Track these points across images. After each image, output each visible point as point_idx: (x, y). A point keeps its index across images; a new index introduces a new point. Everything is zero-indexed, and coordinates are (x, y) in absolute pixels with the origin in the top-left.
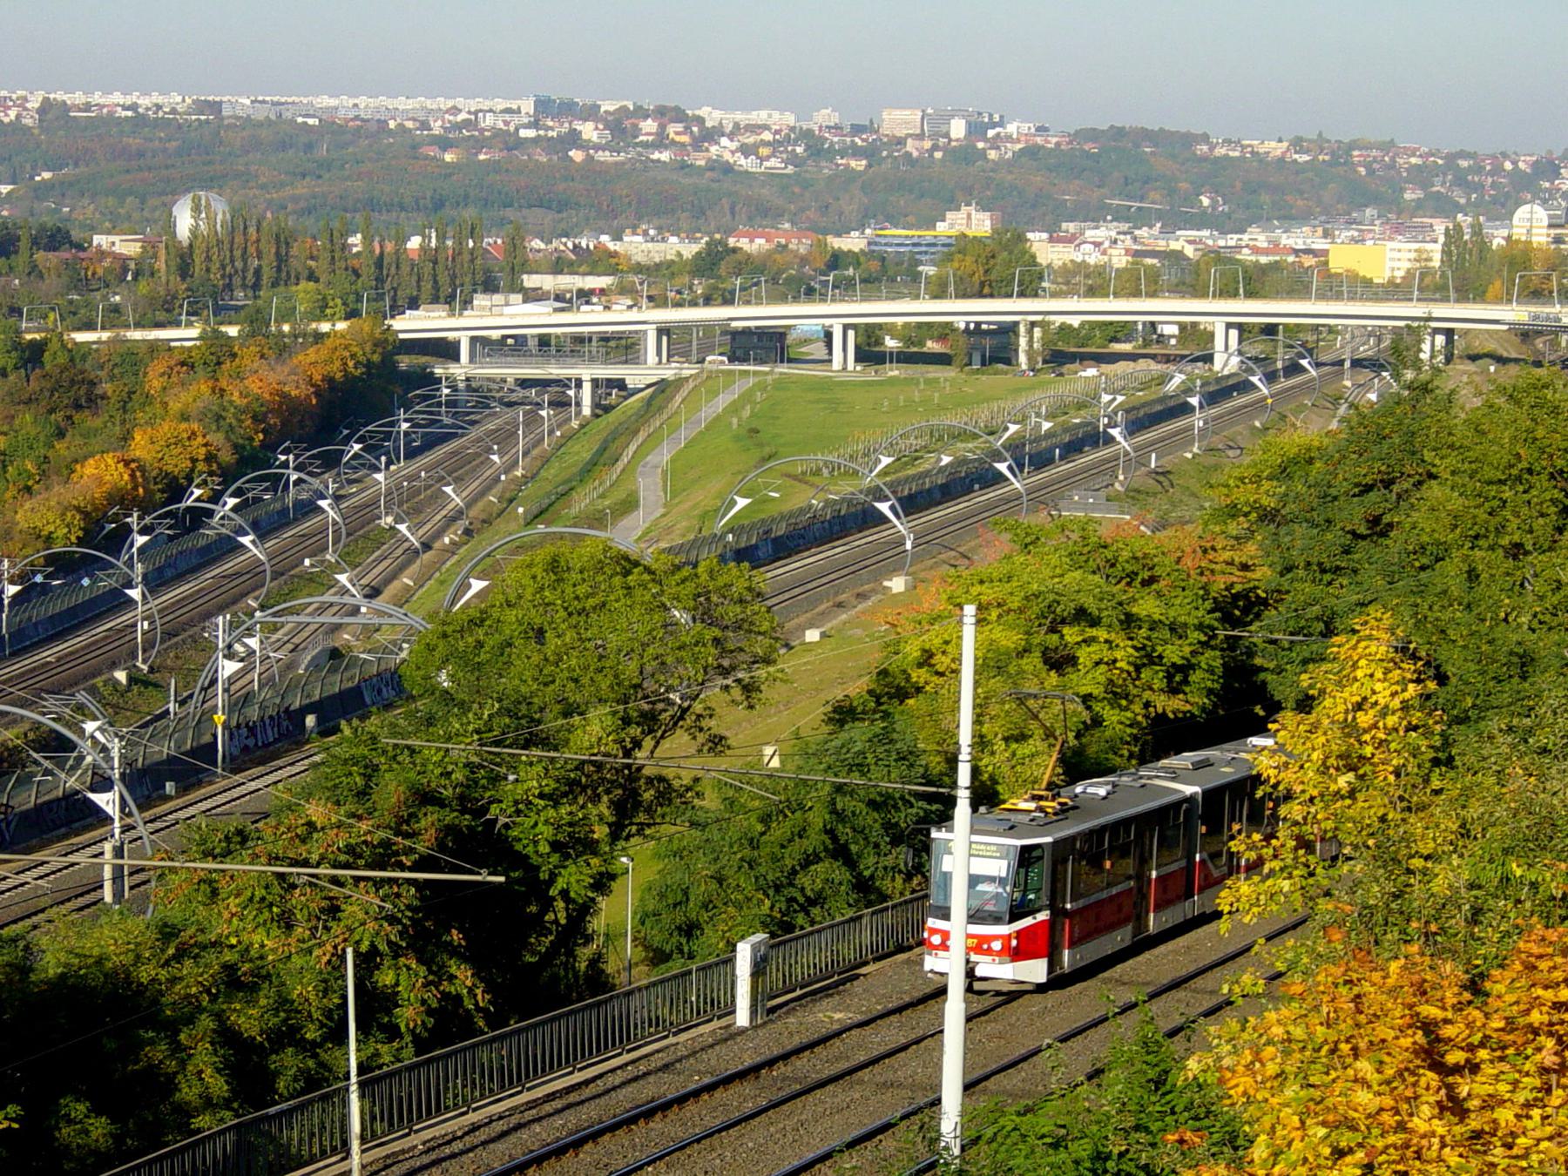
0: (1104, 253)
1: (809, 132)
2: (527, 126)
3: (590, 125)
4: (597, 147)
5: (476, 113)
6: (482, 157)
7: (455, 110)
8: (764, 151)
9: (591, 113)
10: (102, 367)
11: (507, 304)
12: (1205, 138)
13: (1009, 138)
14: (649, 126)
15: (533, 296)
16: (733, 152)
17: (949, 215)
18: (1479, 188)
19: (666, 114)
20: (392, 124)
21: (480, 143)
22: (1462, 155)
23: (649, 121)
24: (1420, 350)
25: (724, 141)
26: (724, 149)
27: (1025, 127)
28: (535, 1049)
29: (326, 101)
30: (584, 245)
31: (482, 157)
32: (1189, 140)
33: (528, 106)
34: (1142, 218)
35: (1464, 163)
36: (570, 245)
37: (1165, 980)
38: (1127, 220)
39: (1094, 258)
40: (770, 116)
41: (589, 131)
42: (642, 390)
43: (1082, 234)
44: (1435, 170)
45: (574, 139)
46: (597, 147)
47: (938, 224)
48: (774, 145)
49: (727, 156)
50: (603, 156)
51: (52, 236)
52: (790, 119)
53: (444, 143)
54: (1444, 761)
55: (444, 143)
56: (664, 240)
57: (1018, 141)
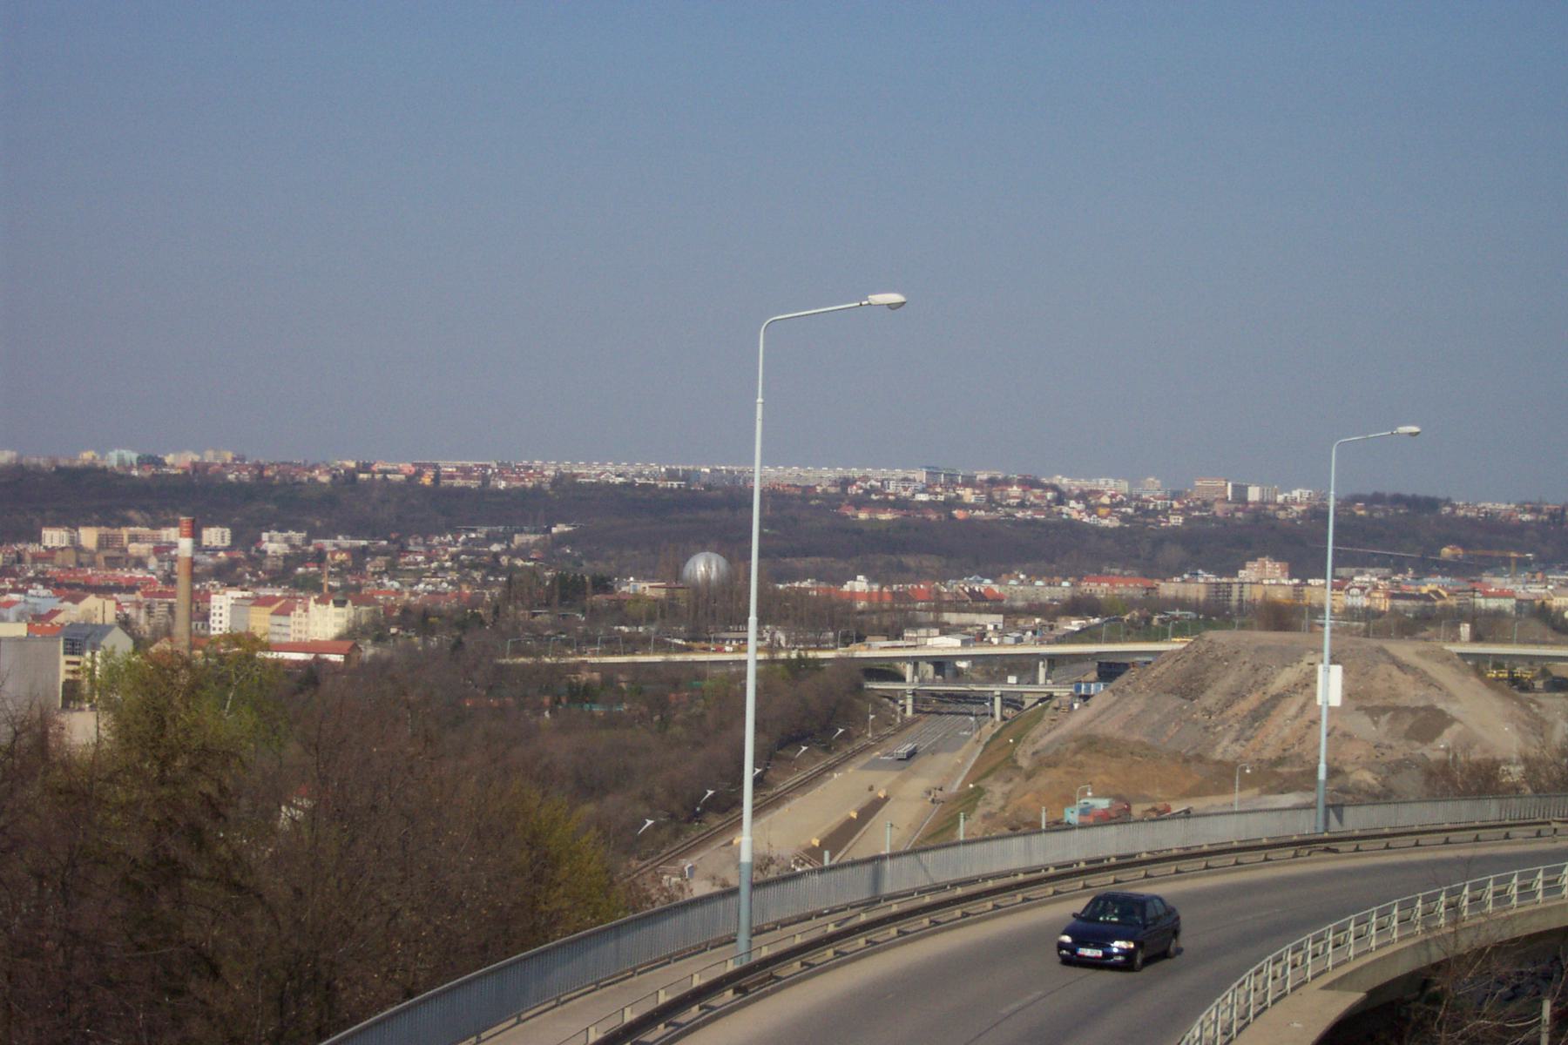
0: (1368, 595)
2: (923, 491)
5: (882, 482)
7: (866, 479)
10: (692, 869)
11: (928, 637)
13: (1294, 502)
14: (1015, 490)
15: (946, 630)
16: (1079, 512)
17: (1249, 564)
19: (1029, 483)
20: (819, 489)
21: (885, 504)
23: (1015, 488)
24: (672, 488)
25: (1072, 503)
26: (1073, 510)
27: (1306, 493)
29: (1489, 506)
30: (977, 589)
33: (921, 476)
34: (1399, 567)
36: (967, 589)
39: (1362, 602)
40: (1107, 483)
41: (968, 495)
43: (1352, 579)
45: (957, 503)
46: (974, 507)
47: (1240, 572)
48: (1113, 506)
49: (1075, 515)
50: (980, 513)
52: (1124, 486)
53: (860, 502)
54: (1187, 761)
55: (860, 502)
57: (1301, 504)
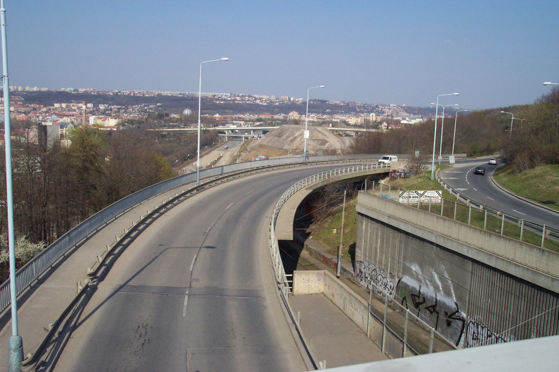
1: (270, 99)
3: (238, 98)
4: (239, 101)
6: (469, 183)
8: (264, 102)
9: (238, 96)
12: (328, 101)
13: (300, 100)
18: (368, 109)
21: (222, 100)
22: (365, 104)
25: (258, 100)
26: (258, 102)
28: (6, 290)
31: (469, 183)
32: (325, 101)
33: (229, 95)
34: (319, 113)
35: (366, 106)
37: (296, 346)
38: (316, 113)
41: (238, 98)
42: (378, 197)
44: (361, 106)
46: (239, 101)
49: (258, 103)
51: (345, 188)
53: (217, 100)
55: (217, 100)
56: (250, 116)
